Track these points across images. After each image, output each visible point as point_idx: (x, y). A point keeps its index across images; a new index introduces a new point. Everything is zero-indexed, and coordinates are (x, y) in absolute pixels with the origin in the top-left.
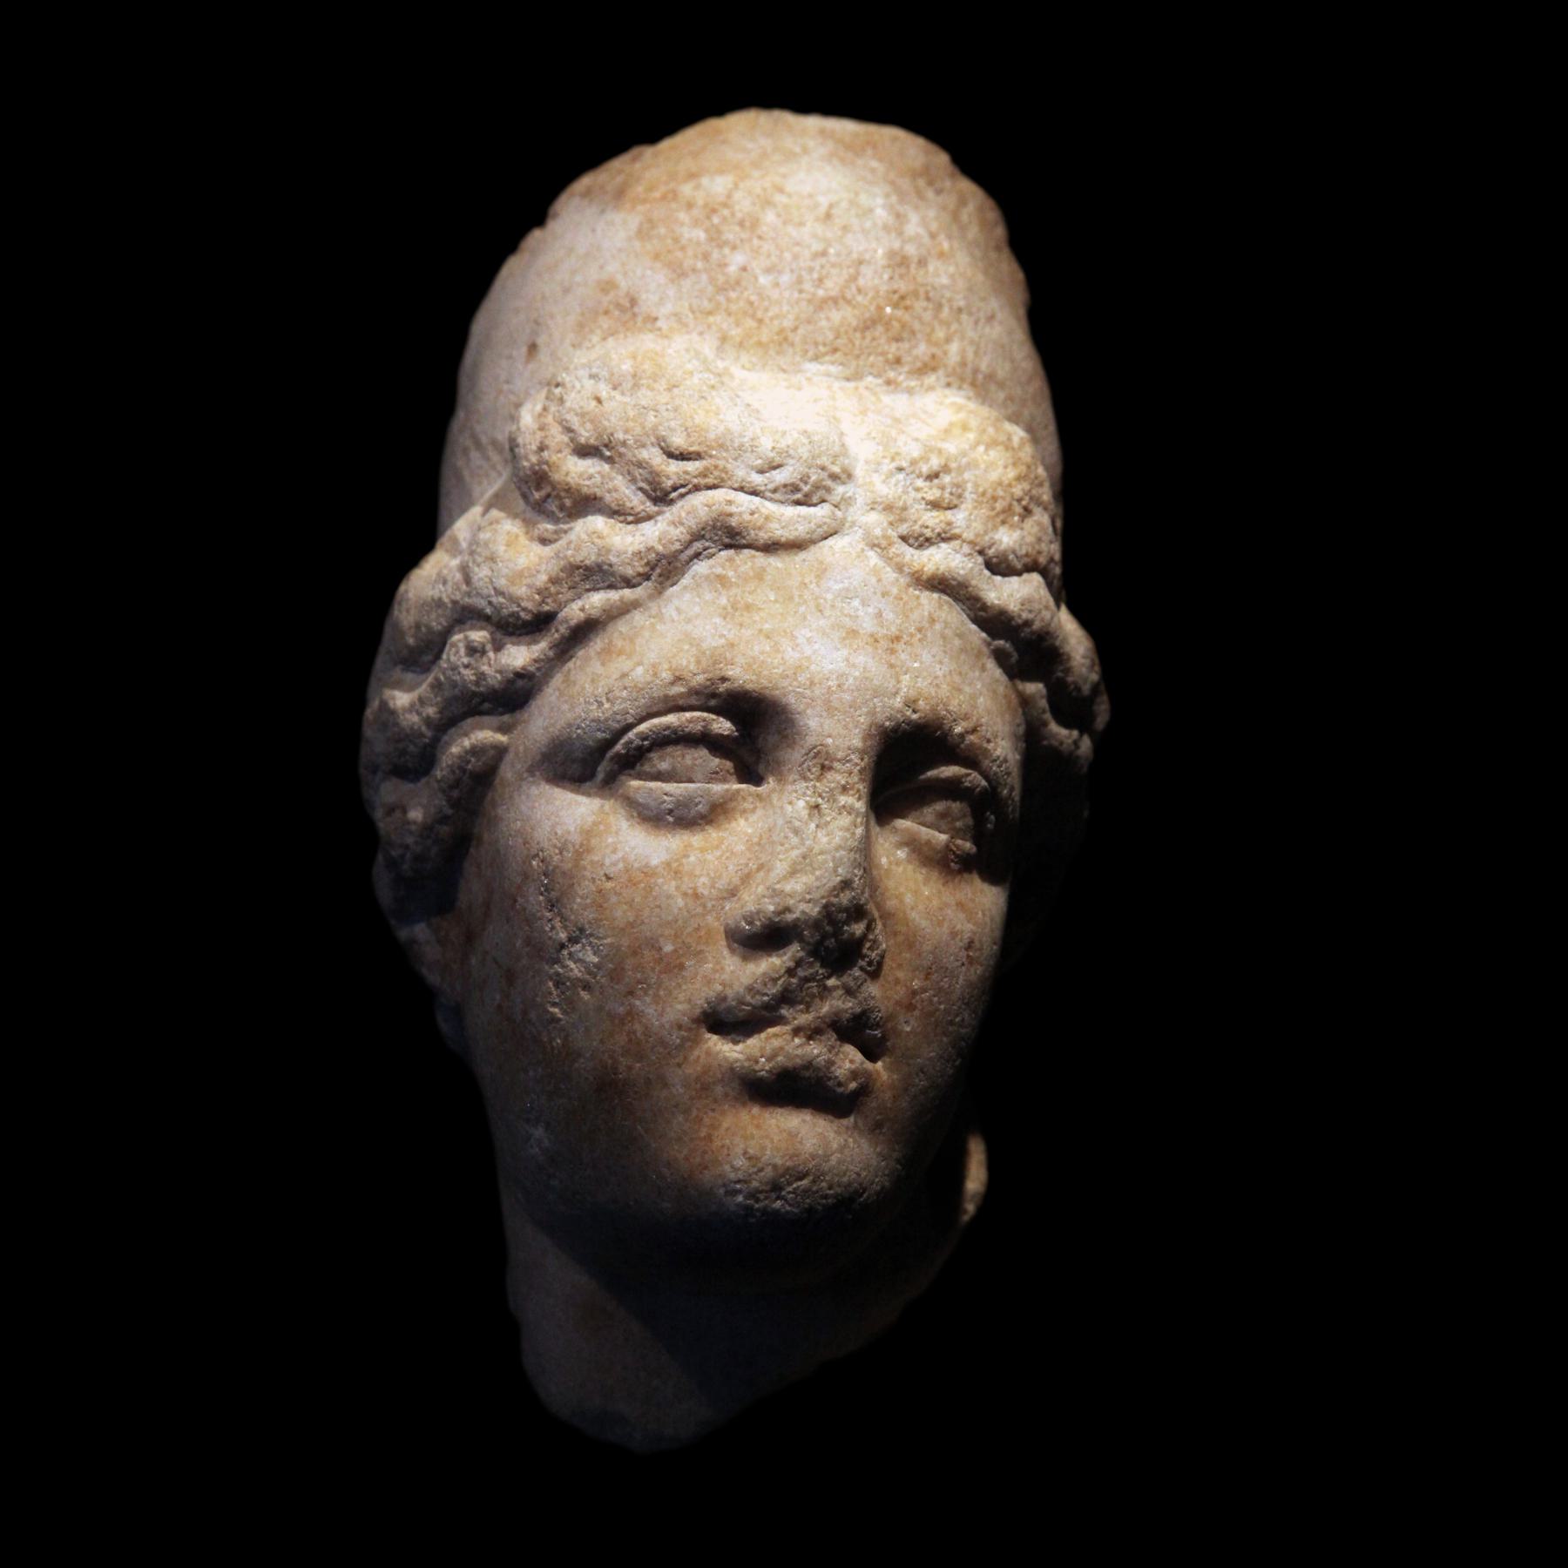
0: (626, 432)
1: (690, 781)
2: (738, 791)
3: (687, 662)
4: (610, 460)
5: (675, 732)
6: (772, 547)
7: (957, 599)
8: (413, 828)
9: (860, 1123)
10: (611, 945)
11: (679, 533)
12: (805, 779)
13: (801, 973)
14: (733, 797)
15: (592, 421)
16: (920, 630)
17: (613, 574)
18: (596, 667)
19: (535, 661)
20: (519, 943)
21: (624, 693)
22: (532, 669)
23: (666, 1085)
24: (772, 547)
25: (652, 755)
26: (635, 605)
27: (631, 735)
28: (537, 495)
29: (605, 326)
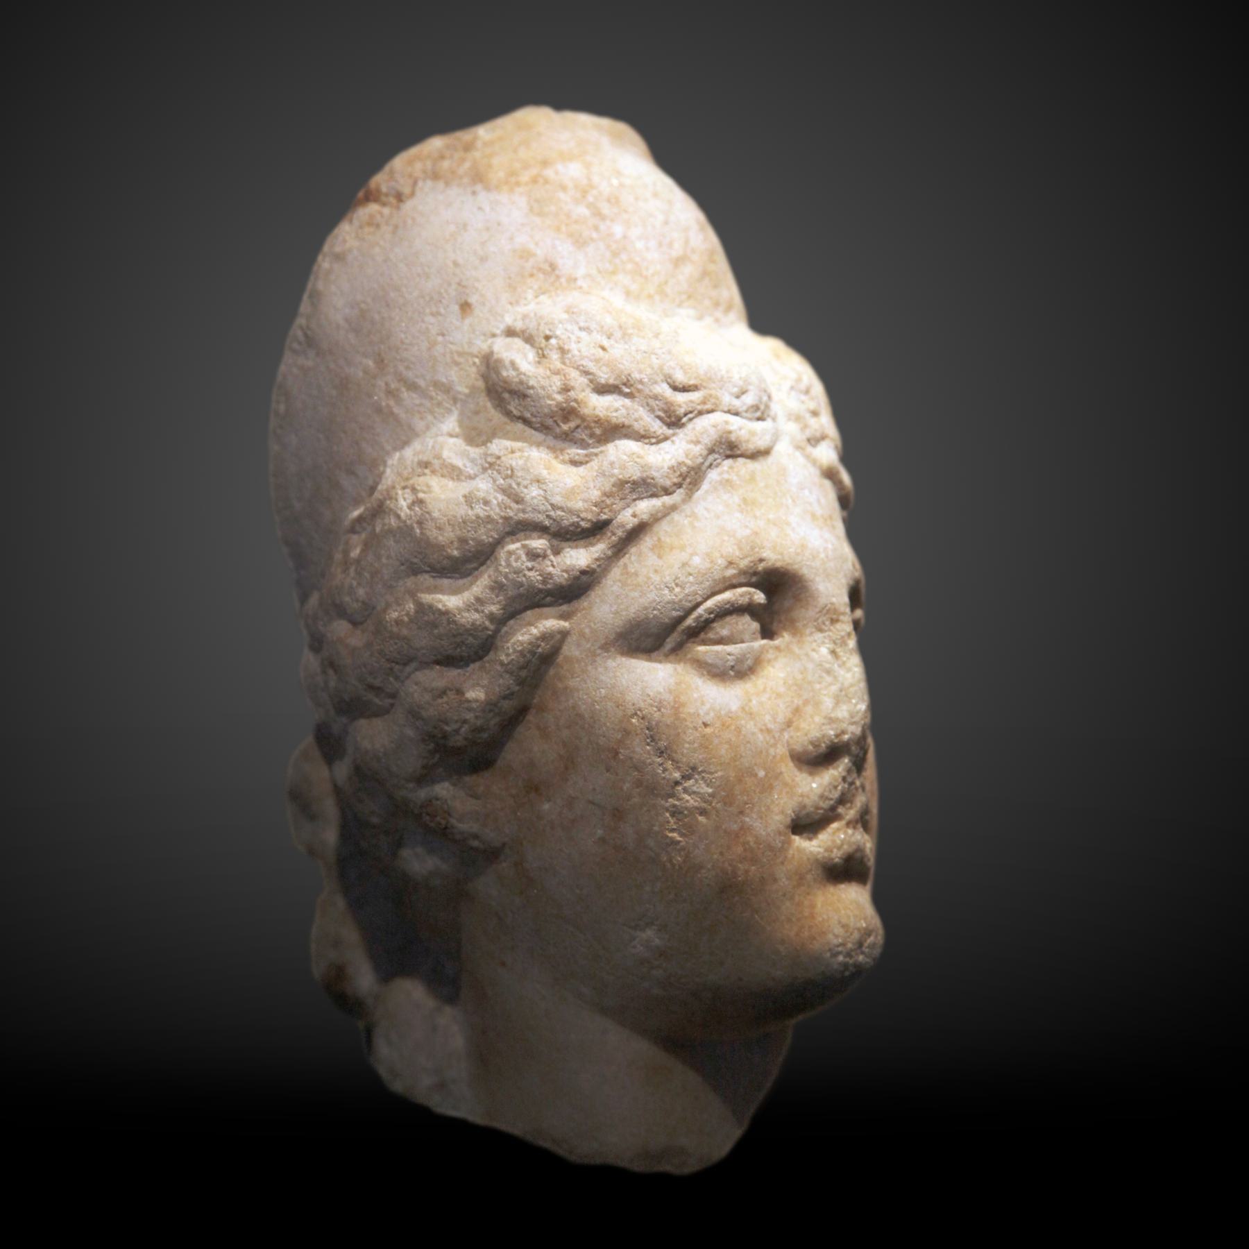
0: (640, 372)
1: (742, 642)
2: (763, 647)
3: (731, 549)
4: (630, 396)
5: (732, 605)
8: (474, 705)
10: (721, 777)
11: (698, 450)
12: (821, 630)
14: (763, 650)
15: (607, 365)
17: (655, 486)
18: (652, 560)
19: (597, 560)
20: (626, 786)
21: (691, 578)
22: (594, 566)
23: (775, 880)
25: (715, 625)
26: (674, 508)
27: (700, 610)
28: (565, 427)
29: (536, 287)
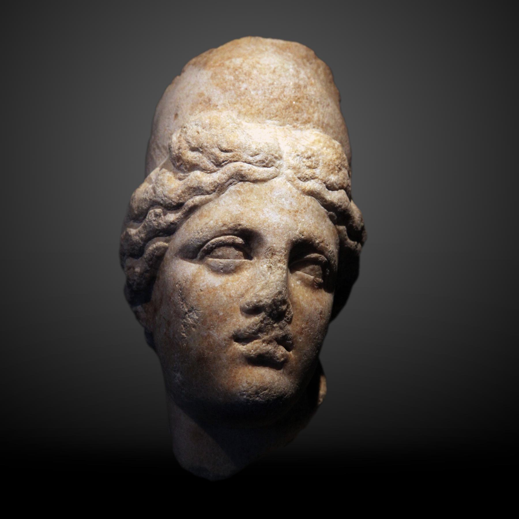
0: (207, 143)
1: (229, 258)
2: (244, 262)
3: (227, 219)
4: (202, 152)
5: (223, 242)
6: (255, 181)
7: (317, 198)
8: (137, 274)
9: (285, 372)
10: (202, 313)
11: (225, 176)
12: (267, 258)
13: (265, 322)
14: (243, 264)
15: (196, 139)
16: (304, 209)
17: (203, 190)
18: (197, 221)
19: (177, 219)
20: (172, 312)
21: (207, 230)
22: (176, 221)
23: (220, 359)
24: (255, 181)
25: (216, 250)
26: (210, 200)
27: (209, 243)
28: (178, 164)
29: (200, 108)
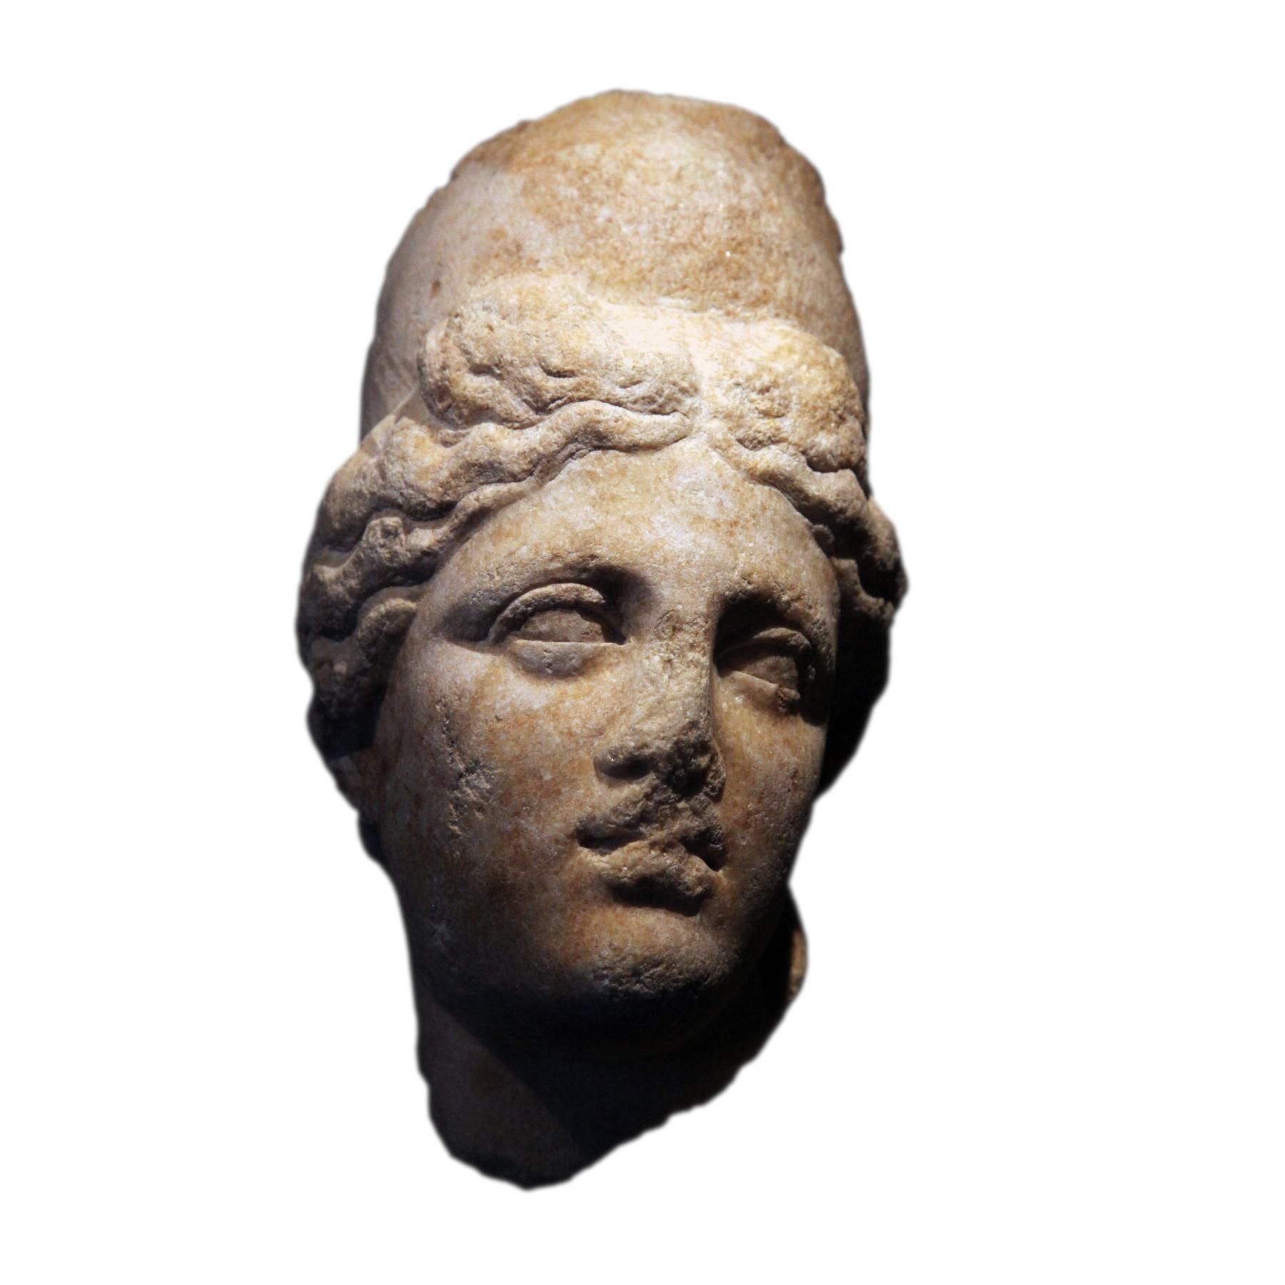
0: (513, 354)
1: (566, 640)
2: (605, 648)
3: (563, 542)
4: (500, 377)
5: (553, 600)
6: (632, 449)
7: (784, 491)
8: (339, 678)
9: (705, 920)
10: (501, 774)
11: (556, 437)
12: (660, 638)
13: (656, 797)
14: (601, 653)
15: (485, 345)
16: (754, 516)
17: (502, 471)
18: (488, 546)
19: (439, 542)
20: (425, 773)
21: (512, 568)
22: (436, 548)
23: (546, 889)
24: (632, 449)
25: (534, 619)
26: (521, 496)
27: (517, 602)
28: (440, 406)
29: (496, 267)
